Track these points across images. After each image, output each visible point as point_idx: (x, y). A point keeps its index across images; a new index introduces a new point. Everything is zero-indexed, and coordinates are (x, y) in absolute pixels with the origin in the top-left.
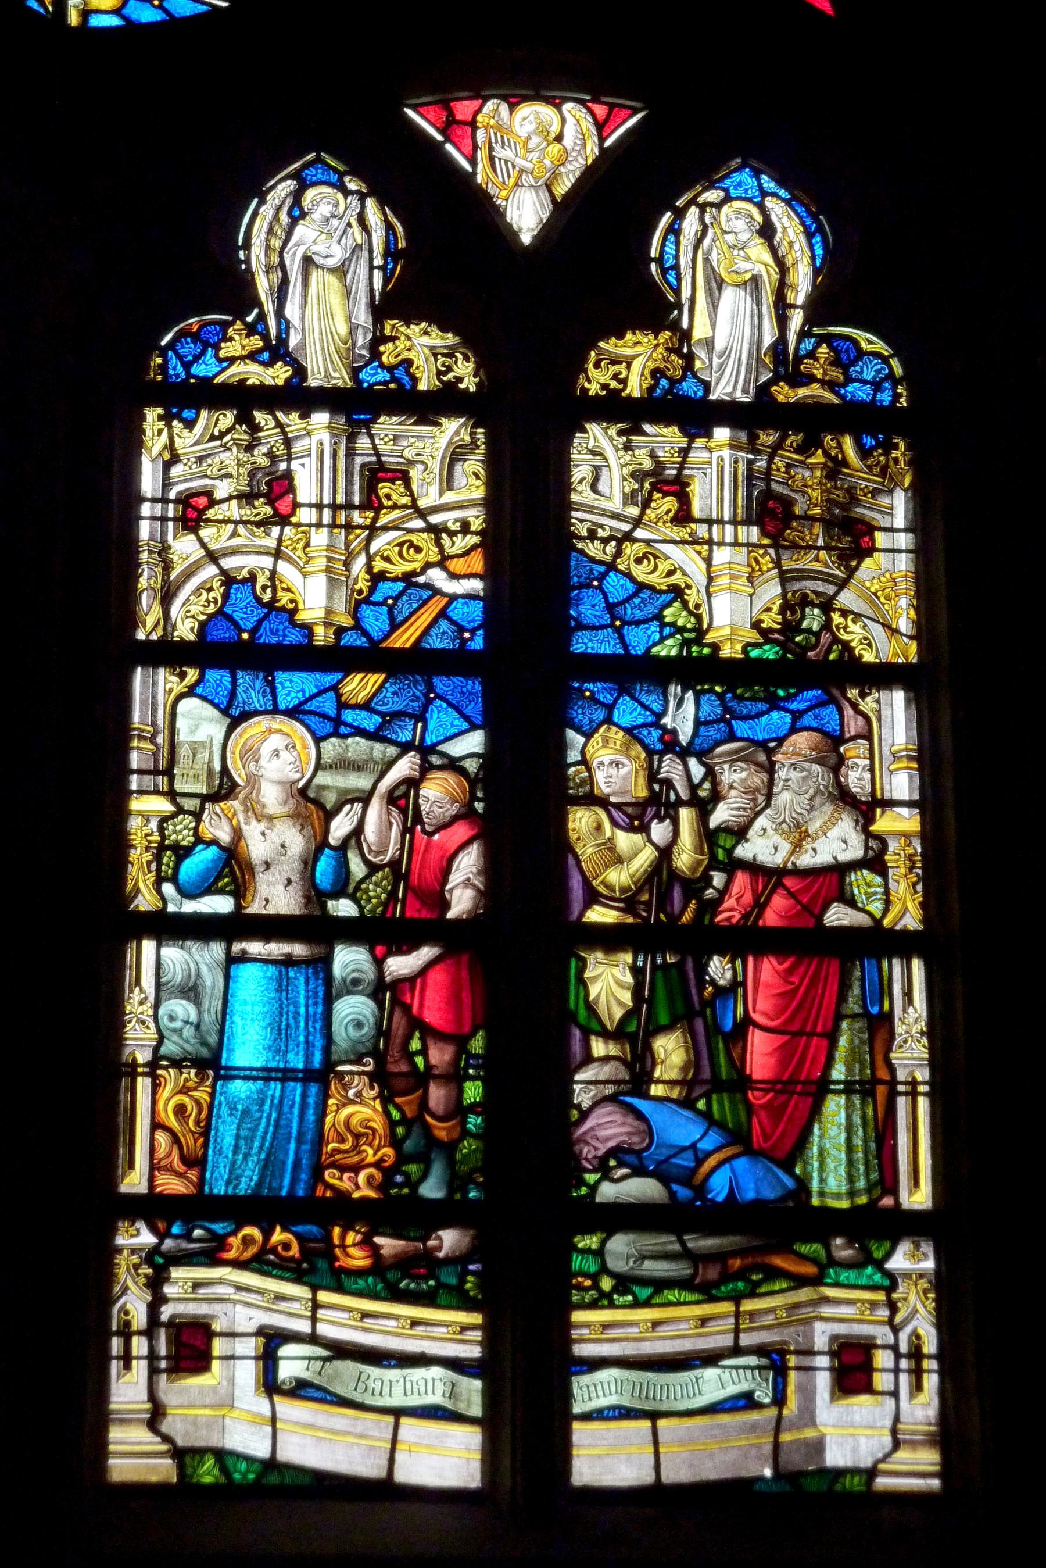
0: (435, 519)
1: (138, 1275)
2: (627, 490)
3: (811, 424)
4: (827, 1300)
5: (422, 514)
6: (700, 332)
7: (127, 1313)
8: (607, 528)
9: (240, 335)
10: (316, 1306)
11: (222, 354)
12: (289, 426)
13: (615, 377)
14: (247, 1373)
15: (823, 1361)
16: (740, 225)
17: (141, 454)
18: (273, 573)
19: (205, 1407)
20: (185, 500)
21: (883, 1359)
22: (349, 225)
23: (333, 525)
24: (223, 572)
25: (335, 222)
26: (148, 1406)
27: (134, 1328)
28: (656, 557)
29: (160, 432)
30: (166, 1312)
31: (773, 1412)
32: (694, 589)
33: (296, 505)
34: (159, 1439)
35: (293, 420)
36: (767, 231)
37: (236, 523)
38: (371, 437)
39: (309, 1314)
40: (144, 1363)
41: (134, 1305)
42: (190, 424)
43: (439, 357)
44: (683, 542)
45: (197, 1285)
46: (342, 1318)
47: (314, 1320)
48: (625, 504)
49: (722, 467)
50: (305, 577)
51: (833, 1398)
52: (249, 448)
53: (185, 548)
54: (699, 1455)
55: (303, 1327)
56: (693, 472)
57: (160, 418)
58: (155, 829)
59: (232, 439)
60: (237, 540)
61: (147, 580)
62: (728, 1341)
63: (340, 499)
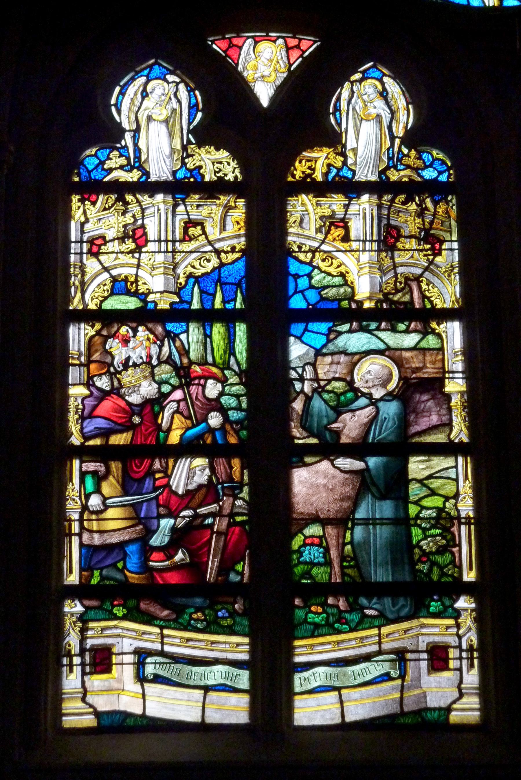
0: (217, 246)
1: (75, 626)
2: (318, 226)
3: (412, 189)
4: (424, 626)
5: (210, 243)
6: (351, 144)
7: (70, 645)
8: (308, 246)
9: (115, 157)
10: (163, 636)
11: (106, 167)
12: (143, 202)
13: (310, 168)
14: (129, 672)
15: (424, 656)
16: (371, 90)
17: (71, 220)
18: (137, 275)
19: (192, 701)
20: (91, 241)
21: (453, 653)
22: (170, 98)
23: (166, 252)
24: (111, 276)
25: (163, 97)
26: (81, 690)
27: (73, 652)
28: (332, 258)
29: (79, 207)
30: (89, 643)
31: (399, 682)
32: (351, 274)
33: (147, 241)
34: (88, 706)
35: (145, 199)
36: (384, 94)
37: (117, 253)
38: (186, 206)
39: (160, 640)
40: (79, 668)
41: (73, 641)
42: (94, 203)
43: (215, 163)
44: (346, 251)
45: (103, 629)
46: (177, 641)
47: (162, 643)
48: (317, 233)
49: (365, 213)
50: (153, 277)
51: (429, 673)
52: (124, 214)
53: (92, 265)
54: (362, 706)
55: (158, 647)
56: (352, 217)
57: (79, 200)
58: (80, 402)
59: (115, 209)
60: (118, 260)
61: (75, 281)
62: (376, 648)
63: (170, 238)
